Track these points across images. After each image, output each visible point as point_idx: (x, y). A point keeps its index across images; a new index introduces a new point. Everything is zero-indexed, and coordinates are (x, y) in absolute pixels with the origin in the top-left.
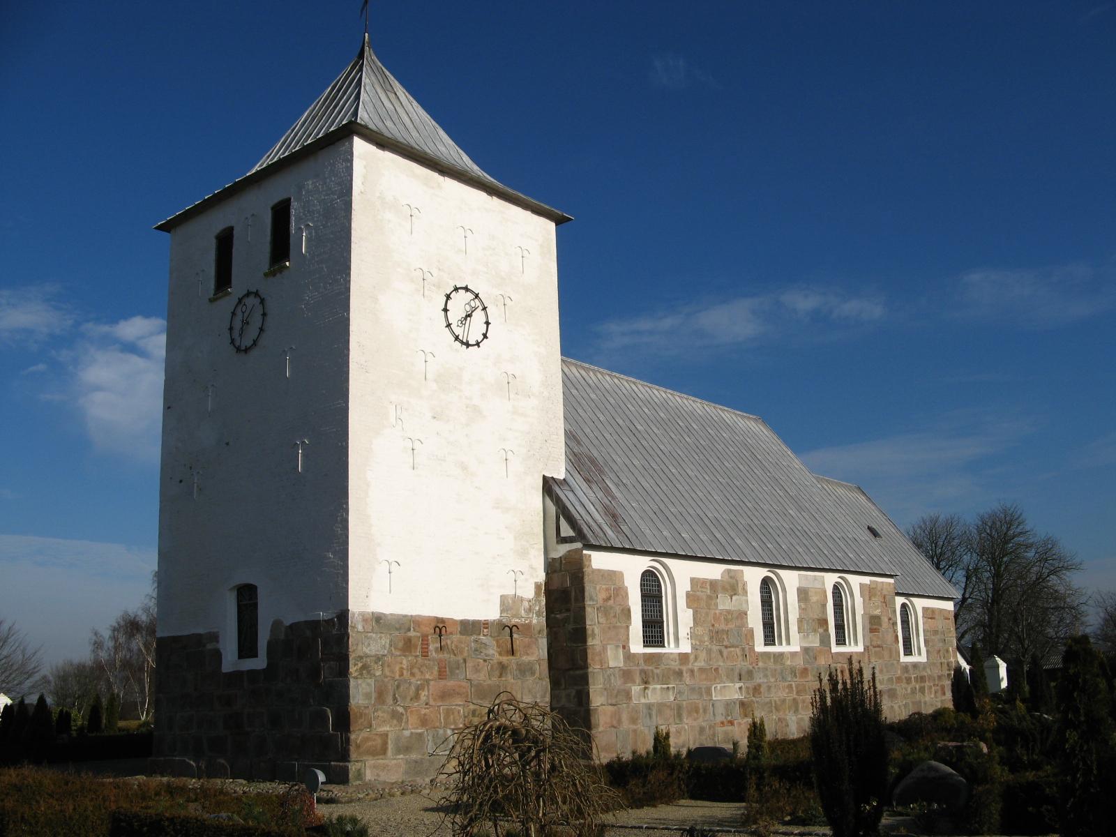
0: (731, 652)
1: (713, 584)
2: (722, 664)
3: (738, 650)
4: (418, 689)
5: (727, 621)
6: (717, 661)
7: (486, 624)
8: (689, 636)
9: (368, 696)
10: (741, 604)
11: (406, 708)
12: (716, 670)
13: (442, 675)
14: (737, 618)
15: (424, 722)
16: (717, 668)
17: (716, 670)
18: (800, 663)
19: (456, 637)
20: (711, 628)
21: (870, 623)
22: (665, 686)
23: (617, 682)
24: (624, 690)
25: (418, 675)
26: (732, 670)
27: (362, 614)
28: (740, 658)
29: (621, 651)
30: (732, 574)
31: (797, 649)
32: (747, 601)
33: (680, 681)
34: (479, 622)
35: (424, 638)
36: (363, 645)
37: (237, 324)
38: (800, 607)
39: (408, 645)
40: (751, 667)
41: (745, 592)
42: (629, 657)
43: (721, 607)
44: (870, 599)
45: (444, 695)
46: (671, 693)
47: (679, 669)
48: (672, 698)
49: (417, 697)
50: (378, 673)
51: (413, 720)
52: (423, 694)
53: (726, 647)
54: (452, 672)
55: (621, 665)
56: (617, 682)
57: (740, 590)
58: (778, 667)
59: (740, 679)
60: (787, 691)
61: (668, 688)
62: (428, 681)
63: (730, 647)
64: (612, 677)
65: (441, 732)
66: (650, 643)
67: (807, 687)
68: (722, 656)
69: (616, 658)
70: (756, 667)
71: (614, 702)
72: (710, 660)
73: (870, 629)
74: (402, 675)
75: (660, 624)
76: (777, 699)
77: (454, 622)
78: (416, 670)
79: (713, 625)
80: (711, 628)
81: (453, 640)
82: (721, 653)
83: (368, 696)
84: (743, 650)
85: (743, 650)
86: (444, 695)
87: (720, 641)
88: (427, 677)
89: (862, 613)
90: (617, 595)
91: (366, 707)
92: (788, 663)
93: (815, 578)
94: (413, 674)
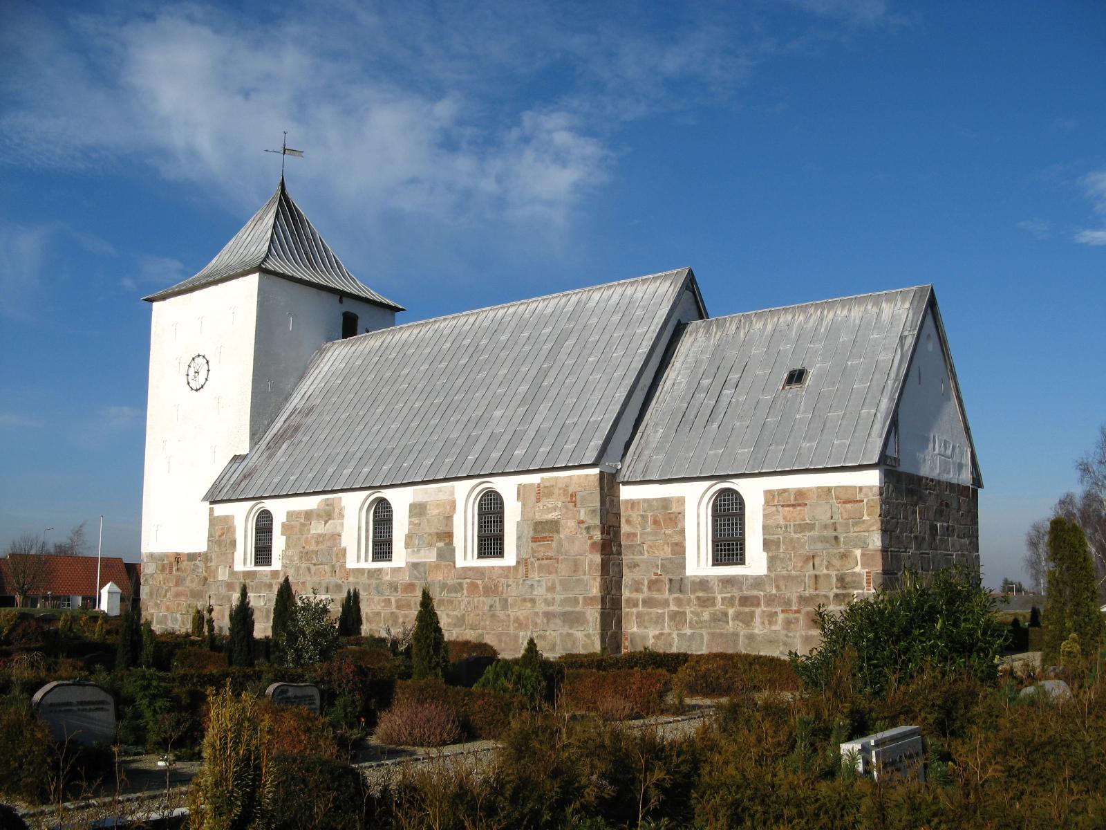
0: (319, 569)
1: (308, 515)
2: (309, 579)
3: (326, 567)
4: (167, 591)
5: (317, 543)
6: (305, 576)
7: (200, 554)
8: (281, 557)
9: (147, 594)
10: (336, 528)
11: (161, 601)
12: (303, 583)
13: (177, 585)
14: (329, 539)
15: (168, 609)
16: (304, 582)
17: (303, 583)
18: (406, 578)
19: (185, 563)
20: (302, 550)
21: (535, 530)
22: (258, 594)
23: (223, 591)
24: (227, 596)
25: (167, 585)
26: (319, 583)
27: (146, 553)
28: (329, 574)
29: (228, 569)
30: (328, 502)
31: (403, 565)
32: (342, 524)
33: (270, 591)
34: (196, 553)
35: (171, 564)
36: (148, 569)
37: (192, 372)
38: (410, 523)
39: (163, 569)
40: (340, 582)
41: (341, 516)
42: (233, 573)
43: (313, 532)
44: (538, 500)
45: (177, 595)
46: (262, 599)
47: (270, 582)
48: (262, 604)
49: (165, 596)
50: (151, 583)
51: (163, 608)
52: (168, 594)
53: (315, 565)
54: (182, 583)
55: (226, 579)
56: (223, 591)
57: (335, 515)
58: (374, 582)
59: (327, 592)
60: (383, 604)
61: (260, 596)
62: (170, 587)
63: (319, 565)
64: (220, 587)
65: (174, 615)
66: (491, 554)
67: (412, 603)
68: (310, 573)
69: (224, 574)
70: (346, 582)
71: (220, 603)
72: (298, 575)
73: (532, 538)
74: (160, 583)
75: (389, 543)
76: (369, 612)
77: (184, 554)
78: (166, 581)
79: (304, 547)
80: (302, 550)
81: (185, 564)
82: (309, 569)
83: (147, 594)
84: (333, 566)
85: (333, 566)
86: (177, 595)
87: (309, 560)
88: (171, 585)
89: (519, 519)
90: (228, 531)
91: (146, 600)
92: (388, 578)
93: (440, 490)
94: (164, 583)
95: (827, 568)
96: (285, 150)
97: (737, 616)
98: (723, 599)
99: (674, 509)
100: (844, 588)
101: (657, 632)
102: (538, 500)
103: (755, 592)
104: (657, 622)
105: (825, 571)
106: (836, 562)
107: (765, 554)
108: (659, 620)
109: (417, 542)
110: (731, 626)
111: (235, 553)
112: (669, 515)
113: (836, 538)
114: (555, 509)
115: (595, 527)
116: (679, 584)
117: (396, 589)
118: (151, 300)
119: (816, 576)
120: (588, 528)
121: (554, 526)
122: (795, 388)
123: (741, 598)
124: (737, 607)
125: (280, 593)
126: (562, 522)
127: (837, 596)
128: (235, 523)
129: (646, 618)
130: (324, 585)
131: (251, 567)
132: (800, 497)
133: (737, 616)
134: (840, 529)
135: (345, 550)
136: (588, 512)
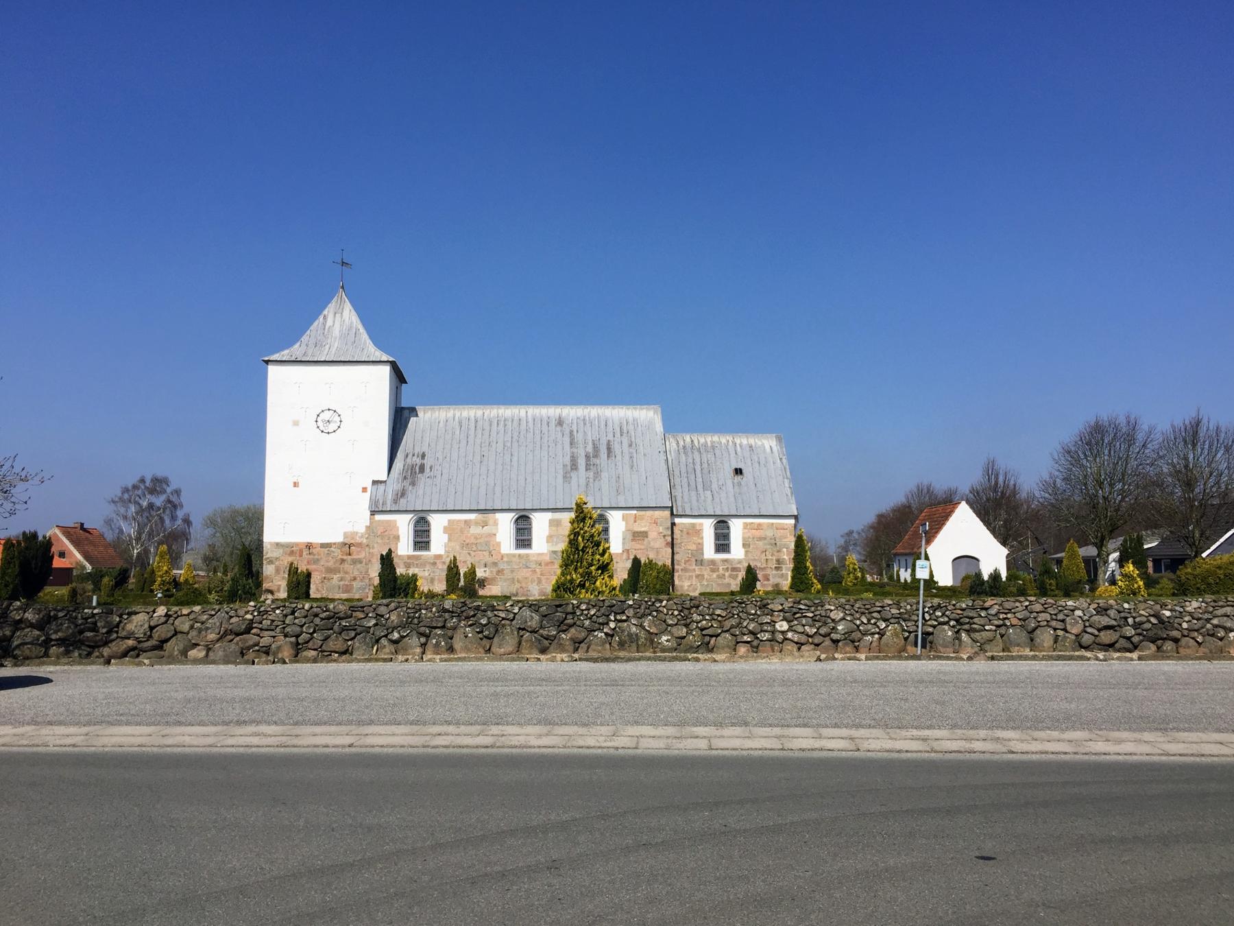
21: (634, 536)
53: (474, 551)
89: (624, 530)
95: (772, 556)
96: (343, 262)
97: (730, 576)
98: (723, 569)
99: (698, 528)
100: (779, 564)
101: (689, 584)
102: (635, 522)
103: (738, 566)
104: (689, 579)
105: (771, 557)
106: (775, 554)
107: (743, 549)
108: (690, 578)
109: (555, 540)
110: (727, 580)
111: (399, 544)
112: (697, 532)
113: (776, 544)
114: (645, 526)
115: (668, 535)
116: (700, 562)
117: (540, 564)
118: (267, 362)
119: (767, 559)
120: (664, 536)
121: (644, 535)
122: (744, 471)
123: (732, 568)
124: (730, 572)
125: (450, 569)
126: (649, 533)
127: (776, 567)
128: (398, 525)
129: (683, 577)
130: (483, 562)
131: (411, 552)
132: (759, 526)
133: (730, 576)
134: (777, 540)
135: (500, 543)
136: (664, 529)
